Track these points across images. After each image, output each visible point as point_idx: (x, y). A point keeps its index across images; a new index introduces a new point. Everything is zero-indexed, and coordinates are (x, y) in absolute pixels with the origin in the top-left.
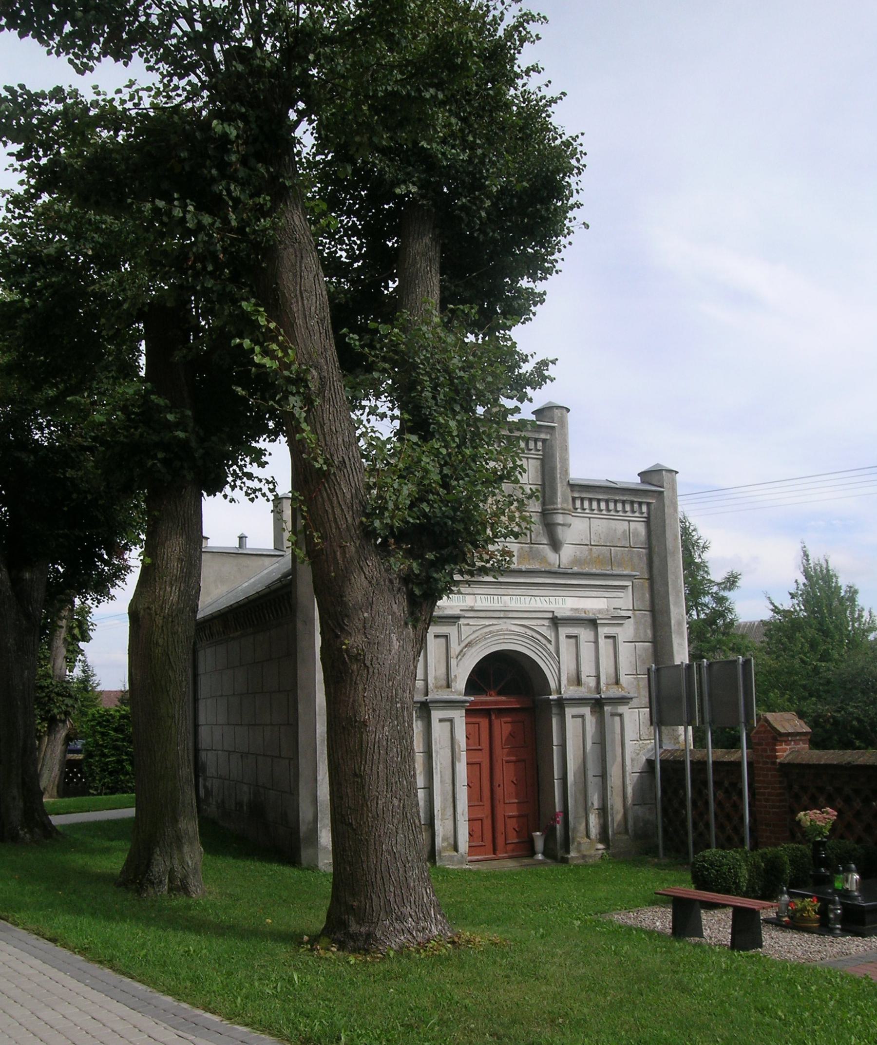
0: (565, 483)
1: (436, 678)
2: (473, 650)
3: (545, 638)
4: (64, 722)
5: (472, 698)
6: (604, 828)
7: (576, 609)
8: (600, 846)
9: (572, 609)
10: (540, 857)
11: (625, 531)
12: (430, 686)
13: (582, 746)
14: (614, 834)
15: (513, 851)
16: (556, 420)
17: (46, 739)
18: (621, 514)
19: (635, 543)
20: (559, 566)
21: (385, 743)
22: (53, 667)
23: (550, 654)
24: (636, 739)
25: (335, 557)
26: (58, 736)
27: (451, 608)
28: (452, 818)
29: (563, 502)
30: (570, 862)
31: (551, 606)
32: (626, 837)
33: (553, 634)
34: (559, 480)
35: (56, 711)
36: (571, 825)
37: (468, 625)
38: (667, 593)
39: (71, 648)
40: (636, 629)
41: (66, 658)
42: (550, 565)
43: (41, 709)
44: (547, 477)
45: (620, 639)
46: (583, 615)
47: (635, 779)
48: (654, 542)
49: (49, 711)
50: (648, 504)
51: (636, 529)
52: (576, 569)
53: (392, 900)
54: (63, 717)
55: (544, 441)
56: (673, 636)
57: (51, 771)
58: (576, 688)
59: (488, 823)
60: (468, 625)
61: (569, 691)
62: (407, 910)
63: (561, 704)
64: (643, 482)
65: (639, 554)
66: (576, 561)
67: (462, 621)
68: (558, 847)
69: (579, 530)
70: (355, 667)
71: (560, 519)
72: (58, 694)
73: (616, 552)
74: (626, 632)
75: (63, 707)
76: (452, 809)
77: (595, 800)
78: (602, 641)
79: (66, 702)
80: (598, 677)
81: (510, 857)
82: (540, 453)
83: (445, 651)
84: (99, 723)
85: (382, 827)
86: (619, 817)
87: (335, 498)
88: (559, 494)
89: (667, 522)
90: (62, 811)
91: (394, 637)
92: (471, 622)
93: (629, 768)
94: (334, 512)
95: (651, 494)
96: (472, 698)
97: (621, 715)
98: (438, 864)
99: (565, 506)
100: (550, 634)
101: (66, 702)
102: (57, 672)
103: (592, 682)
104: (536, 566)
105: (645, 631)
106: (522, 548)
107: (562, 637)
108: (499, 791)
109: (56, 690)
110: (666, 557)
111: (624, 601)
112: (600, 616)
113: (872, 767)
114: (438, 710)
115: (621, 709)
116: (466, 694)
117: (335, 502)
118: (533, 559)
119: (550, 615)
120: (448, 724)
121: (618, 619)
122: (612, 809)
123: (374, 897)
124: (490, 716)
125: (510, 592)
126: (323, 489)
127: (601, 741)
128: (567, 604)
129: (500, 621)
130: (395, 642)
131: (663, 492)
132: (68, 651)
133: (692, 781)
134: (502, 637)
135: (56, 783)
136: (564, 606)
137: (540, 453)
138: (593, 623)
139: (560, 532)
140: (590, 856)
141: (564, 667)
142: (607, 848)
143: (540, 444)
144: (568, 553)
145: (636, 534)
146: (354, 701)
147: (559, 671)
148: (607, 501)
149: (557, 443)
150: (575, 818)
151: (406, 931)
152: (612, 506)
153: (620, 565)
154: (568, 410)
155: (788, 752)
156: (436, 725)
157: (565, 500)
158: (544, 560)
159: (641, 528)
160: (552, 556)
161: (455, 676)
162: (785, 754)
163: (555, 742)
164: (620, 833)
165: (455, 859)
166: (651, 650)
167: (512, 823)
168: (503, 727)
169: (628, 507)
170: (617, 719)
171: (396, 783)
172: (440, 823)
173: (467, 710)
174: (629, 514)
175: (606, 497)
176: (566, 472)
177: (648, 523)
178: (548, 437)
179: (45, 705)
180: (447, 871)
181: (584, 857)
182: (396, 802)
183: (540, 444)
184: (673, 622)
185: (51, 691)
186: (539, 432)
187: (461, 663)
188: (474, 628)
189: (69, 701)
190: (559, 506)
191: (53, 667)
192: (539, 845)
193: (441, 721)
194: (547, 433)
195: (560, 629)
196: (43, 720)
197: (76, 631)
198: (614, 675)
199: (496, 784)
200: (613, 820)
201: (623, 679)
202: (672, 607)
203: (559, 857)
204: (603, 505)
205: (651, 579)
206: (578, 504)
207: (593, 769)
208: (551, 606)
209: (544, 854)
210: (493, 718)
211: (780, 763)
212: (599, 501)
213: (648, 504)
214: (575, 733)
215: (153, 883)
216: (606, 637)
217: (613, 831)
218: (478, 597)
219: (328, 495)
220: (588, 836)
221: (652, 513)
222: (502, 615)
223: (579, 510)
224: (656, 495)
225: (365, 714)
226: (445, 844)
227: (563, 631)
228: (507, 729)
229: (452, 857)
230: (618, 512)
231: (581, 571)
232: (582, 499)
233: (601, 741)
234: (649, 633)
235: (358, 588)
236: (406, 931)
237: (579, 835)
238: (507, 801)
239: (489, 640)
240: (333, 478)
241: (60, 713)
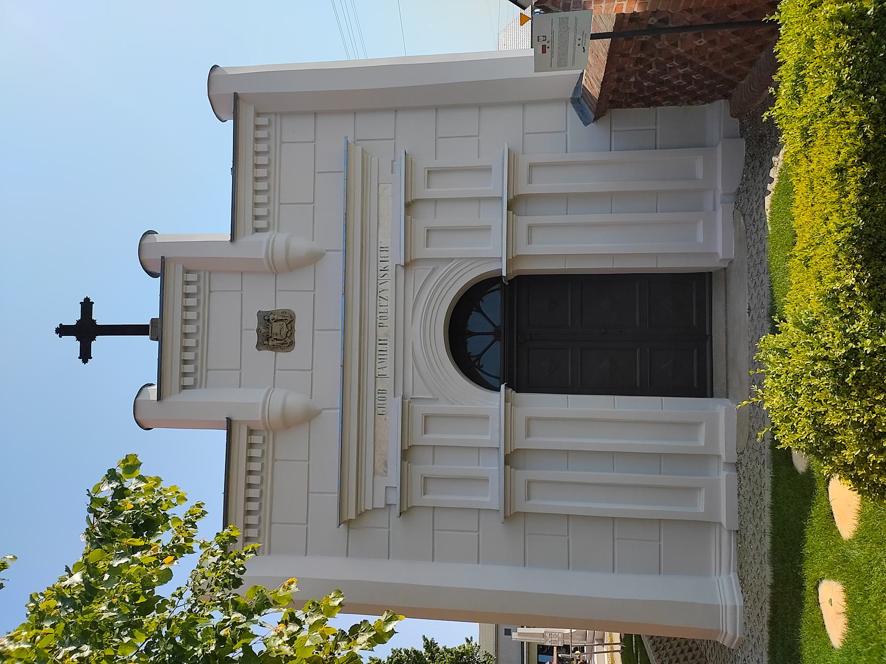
67: (410, 394)
147: (471, 258)
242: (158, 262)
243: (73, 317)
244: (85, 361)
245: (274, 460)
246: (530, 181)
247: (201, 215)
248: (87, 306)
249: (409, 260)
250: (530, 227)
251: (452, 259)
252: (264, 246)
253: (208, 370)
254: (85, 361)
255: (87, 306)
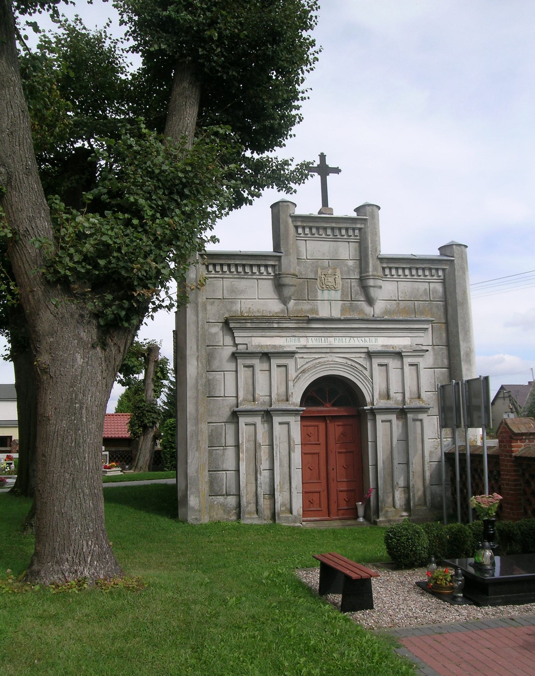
0: (375, 258)
1: (278, 395)
2: (306, 375)
3: (362, 366)
4: (152, 427)
5: (304, 408)
6: (408, 501)
7: (386, 346)
8: (405, 514)
9: (382, 346)
10: (361, 519)
11: (426, 289)
12: (273, 400)
13: (390, 443)
14: (415, 505)
15: (343, 514)
16: (368, 213)
17: (142, 438)
18: (422, 277)
19: (434, 298)
20: (373, 316)
21: (62, 433)
22: (146, 395)
23: (365, 377)
24: (432, 438)
25: (28, 300)
26: (149, 436)
27: (289, 346)
28: (289, 490)
29: (373, 271)
30: (378, 524)
31: (366, 343)
32: (425, 508)
33: (368, 364)
34: (370, 255)
35: (146, 421)
36: (381, 498)
37: (303, 358)
38: (457, 332)
39: (156, 384)
40: (435, 359)
41: (153, 390)
42: (366, 315)
43: (139, 420)
44: (362, 254)
45: (421, 366)
46: (391, 350)
47: (434, 466)
48: (448, 297)
49: (143, 422)
50: (444, 270)
51: (435, 288)
52: (386, 317)
53: (57, 548)
54: (151, 425)
55: (360, 229)
56: (463, 363)
57: (145, 457)
58: (385, 401)
59: (324, 495)
60: (303, 358)
61: (380, 403)
62: (64, 556)
63: (373, 412)
64: (441, 254)
65: (437, 306)
66: (386, 312)
67: (297, 356)
68: (372, 514)
69: (388, 292)
70: (45, 378)
71: (371, 282)
72: (148, 411)
73: (419, 305)
74: (426, 361)
75: (151, 419)
76: (288, 484)
77: (401, 481)
78: (407, 368)
79: (152, 416)
80: (404, 393)
81: (340, 519)
82: (358, 238)
83: (285, 376)
84: (170, 429)
85: (55, 494)
86: (420, 493)
87: (24, 257)
88: (371, 265)
89: (457, 281)
90: (117, 480)
91: (78, 356)
92: (305, 356)
93: (427, 459)
94: (24, 267)
95: (444, 262)
96: (304, 408)
97: (421, 420)
98: (277, 522)
99: (375, 273)
100: (366, 364)
101: (152, 416)
102: (148, 398)
103: (399, 397)
104: (357, 317)
105: (442, 360)
106: (344, 304)
107: (375, 366)
108: (332, 474)
109: (146, 409)
110: (456, 307)
111: (425, 339)
112: (404, 350)
113: (1, 446)
114: (278, 416)
115: (420, 416)
116: (301, 405)
117: (25, 260)
118: (353, 311)
119: (366, 350)
120: (286, 426)
121: (419, 352)
122: (413, 487)
123: (47, 544)
124: (326, 420)
125: (334, 334)
126: (16, 251)
127: (405, 439)
128: (379, 342)
129: (328, 355)
130: (78, 359)
131: (453, 260)
132: (155, 386)
133: (460, 470)
134: (328, 366)
135: (148, 463)
136: (376, 344)
137: (358, 238)
138: (399, 355)
139: (373, 292)
140: (395, 521)
141: (376, 386)
142: (410, 516)
143: (357, 232)
144: (379, 308)
145: (435, 291)
146: (45, 402)
147: (373, 389)
148: (410, 269)
149: (369, 230)
150: (383, 493)
151: (60, 572)
152: (414, 272)
153: (422, 313)
154: (379, 208)
155: (522, 448)
156: (276, 426)
157: (375, 269)
158: (362, 311)
159: (439, 287)
160: (368, 310)
161: (292, 393)
162: (520, 449)
163: (370, 440)
164: (420, 505)
165: (290, 519)
166: (447, 374)
167: (344, 495)
168: (336, 430)
169: (427, 273)
170: (418, 423)
171: (69, 461)
172: (279, 493)
173: (301, 417)
174: (429, 277)
175: (409, 266)
176: (376, 249)
177: (444, 282)
178: (363, 226)
179: (141, 417)
180: (282, 528)
181: (389, 521)
182: (67, 476)
183: (357, 232)
184: (462, 353)
185: (144, 410)
186: (356, 223)
187: (297, 384)
188: (307, 360)
189: (154, 415)
190: (371, 274)
191: (146, 395)
192: (361, 511)
193: (280, 423)
194: (361, 224)
195: (373, 360)
196: (140, 427)
197: (159, 374)
198: (416, 392)
199: (330, 468)
200: (414, 495)
201: (423, 395)
202: (461, 343)
203: (372, 520)
204: (407, 272)
205: (447, 323)
206: (387, 272)
207: (398, 458)
208: (366, 343)
209: (364, 517)
210: (328, 422)
211: (515, 457)
212: (403, 269)
213: (444, 270)
214: (383, 434)
215: (32, 526)
216: (410, 365)
217: (414, 503)
218: (310, 339)
219: (20, 255)
220: (394, 506)
221: (447, 276)
222: (328, 350)
223: (389, 276)
224: (449, 263)
225: (50, 411)
226: (283, 509)
227: (376, 361)
228: (339, 430)
229: (288, 517)
230: (413, 276)
231: (390, 318)
232: (390, 269)
233: (405, 439)
234: (446, 362)
235: (45, 320)
236: (60, 572)
237: (387, 505)
238: (339, 480)
239: (318, 369)
240: (21, 242)
241: (149, 422)
242: (366, 213)
243: (330, 163)
244: (340, 171)
245: (257, 279)
246: (280, 423)
247: (392, 241)
248: (337, 171)
249: (270, 355)
250: (390, 421)
251: (372, 379)
252: (366, 274)
253: (306, 240)
254: (340, 171)
255: (337, 171)
